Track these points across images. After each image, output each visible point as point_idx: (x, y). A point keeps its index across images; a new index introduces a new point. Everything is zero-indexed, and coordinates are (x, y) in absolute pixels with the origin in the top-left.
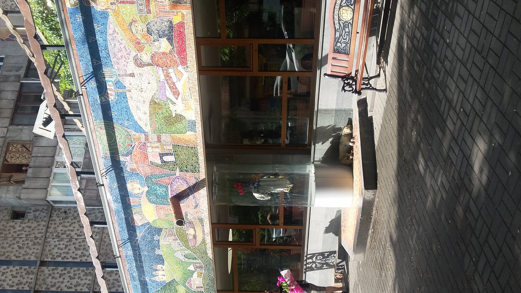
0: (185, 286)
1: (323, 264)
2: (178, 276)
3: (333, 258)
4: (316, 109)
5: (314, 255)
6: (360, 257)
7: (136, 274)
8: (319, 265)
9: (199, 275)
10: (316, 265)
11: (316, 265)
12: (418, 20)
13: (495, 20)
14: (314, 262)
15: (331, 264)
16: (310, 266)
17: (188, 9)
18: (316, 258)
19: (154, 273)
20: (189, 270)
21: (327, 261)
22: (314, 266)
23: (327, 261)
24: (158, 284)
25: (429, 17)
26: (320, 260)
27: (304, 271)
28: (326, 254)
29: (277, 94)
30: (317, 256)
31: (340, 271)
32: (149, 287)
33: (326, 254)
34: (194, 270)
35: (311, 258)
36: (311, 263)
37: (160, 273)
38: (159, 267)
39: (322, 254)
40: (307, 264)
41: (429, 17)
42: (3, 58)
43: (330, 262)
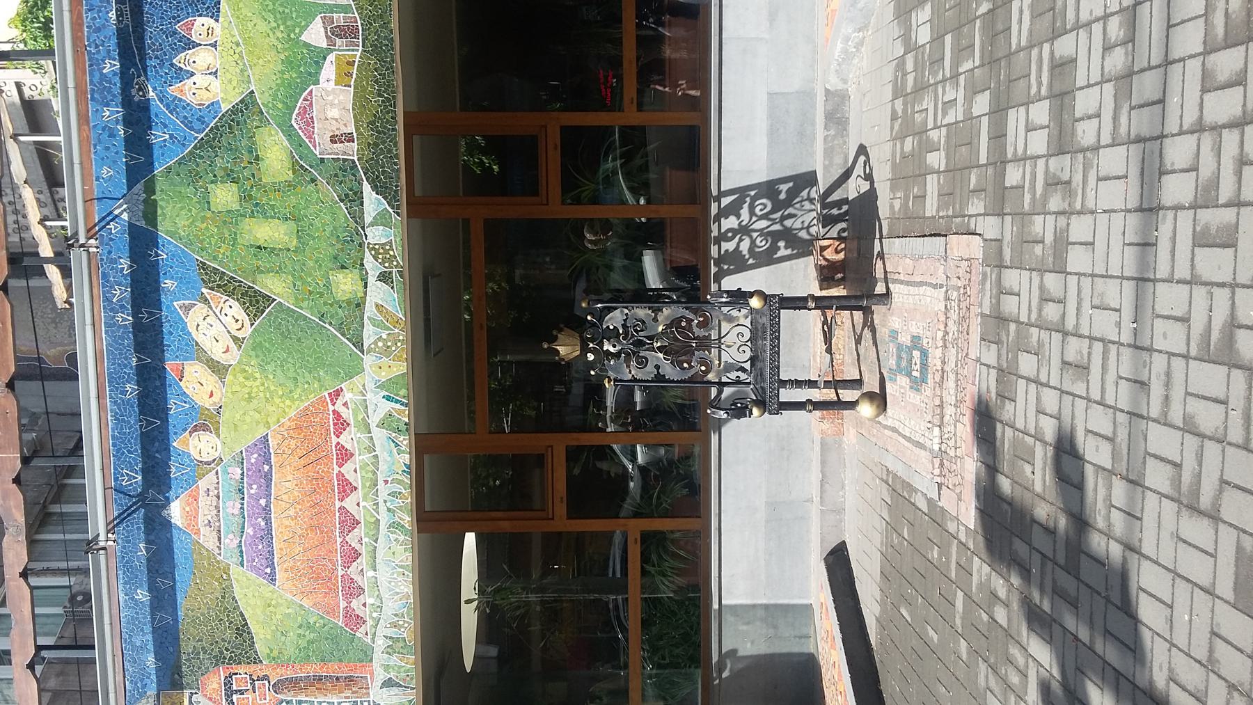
0: (289, 133)
1: (776, 236)
2: (264, 80)
3: (807, 205)
4: (716, 606)
5: (742, 191)
7: (111, 66)
8: (762, 245)
9: (343, 77)
10: (753, 242)
11: (753, 242)
14: (744, 230)
15: (803, 234)
16: (729, 246)
17: (398, 359)
18: (752, 213)
19: (179, 60)
20: (307, 45)
21: (788, 223)
22: (745, 246)
23: (788, 223)
24: (193, 117)
25: (953, 575)
26: (765, 217)
27: (713, 269)
29: (614, 572)
30: (754, 199)
32: (158, 136)
33: (784, 187)
34: (324, 45)
35: (734, 209)
37: (201, 58)
38: (202, 23)
39: (768, 189)
40: (722, 237)
41: (953, 575)
43: (798, 225)
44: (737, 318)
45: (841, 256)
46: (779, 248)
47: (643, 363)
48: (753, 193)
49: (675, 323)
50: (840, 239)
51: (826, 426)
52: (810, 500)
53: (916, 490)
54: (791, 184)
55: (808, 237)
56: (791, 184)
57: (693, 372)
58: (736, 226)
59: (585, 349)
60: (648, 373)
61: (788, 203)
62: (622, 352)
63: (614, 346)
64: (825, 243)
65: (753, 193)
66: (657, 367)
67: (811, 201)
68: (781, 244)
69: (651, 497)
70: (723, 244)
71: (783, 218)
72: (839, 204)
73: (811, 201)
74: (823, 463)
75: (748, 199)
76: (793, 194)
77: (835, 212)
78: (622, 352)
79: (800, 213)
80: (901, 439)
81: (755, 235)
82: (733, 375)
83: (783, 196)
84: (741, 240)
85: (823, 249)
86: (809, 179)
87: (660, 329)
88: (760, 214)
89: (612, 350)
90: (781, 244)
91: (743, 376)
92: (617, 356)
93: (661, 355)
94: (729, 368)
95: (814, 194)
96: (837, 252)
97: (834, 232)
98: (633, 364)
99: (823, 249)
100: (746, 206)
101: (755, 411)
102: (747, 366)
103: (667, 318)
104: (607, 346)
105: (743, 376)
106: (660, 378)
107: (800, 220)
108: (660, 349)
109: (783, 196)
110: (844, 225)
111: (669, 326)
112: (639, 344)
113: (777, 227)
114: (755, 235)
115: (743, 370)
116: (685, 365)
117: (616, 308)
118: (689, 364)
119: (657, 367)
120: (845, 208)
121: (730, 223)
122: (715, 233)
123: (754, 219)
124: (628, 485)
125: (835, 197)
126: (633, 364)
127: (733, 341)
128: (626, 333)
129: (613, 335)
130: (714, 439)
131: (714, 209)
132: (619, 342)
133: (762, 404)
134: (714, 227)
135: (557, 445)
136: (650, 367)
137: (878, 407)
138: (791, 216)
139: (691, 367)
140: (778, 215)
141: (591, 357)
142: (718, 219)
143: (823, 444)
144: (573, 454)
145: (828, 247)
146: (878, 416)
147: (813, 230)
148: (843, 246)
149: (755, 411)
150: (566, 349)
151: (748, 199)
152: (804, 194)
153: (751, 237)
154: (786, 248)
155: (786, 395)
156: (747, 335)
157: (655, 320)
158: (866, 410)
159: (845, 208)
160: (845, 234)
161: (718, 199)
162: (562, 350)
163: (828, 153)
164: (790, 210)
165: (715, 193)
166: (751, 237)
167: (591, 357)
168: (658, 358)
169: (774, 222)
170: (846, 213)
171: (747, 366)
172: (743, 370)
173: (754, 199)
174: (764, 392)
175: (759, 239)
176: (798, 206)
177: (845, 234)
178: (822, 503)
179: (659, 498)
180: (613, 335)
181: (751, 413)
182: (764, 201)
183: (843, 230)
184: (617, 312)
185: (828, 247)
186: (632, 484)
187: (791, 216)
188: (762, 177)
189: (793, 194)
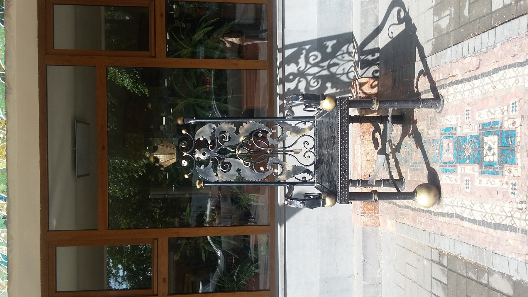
1: (324, 79)
5: (300, 46)
6: (405, 219)
10: (308, 83)
11: (308, 83)
12: (415, 81)
13: (434, 278)
14: (302, 74)
15: (344, 78)
18: (307, 62)
21: (333, 69)
22: (302, 87)
23: (333, 69)
26: (316, 65)
27: (279, 103)
28: (330, 44)
30: (308, 52)
31: (369, 72)
33: (330, 44)
35: (294, 59)
36: (295, 75)
39: (319, 44)
42: (211, 238)
43: (340, 71)
44: (303, 130)
45: (375, 90)
46: (326, 88)
47: (226, 167)
48: (307, 47)
49: (253, 134)
50: (374, 77)
51: (366, 219)
52: (352, 276)
53: (490, 272)
54: (335, 42)
55: (347, 80)
56: (335, 42)
57: (268, 174)
58: (295, 71)
59: (180, 157)
60: (232, 175)
61: (333, 55)
62: (210, 157)
63: (204, 154)
64: (363, 80)
65: (307, 47)
66: (239, 170)
67: (349, 54)
68: (329, 85)
69: (232, 276)
70: (286, 84)
71: (330, 66)
72: (372, 52)
73: (349, 54)
74: (365, 247)
75: (304, 52)
76: (336, 48)
77: (370, 57)
78: (210, 157)
79: (341, 63)
80: (466, 224)
81: (309, 78)
82: (300, 176)
83: (329, 50)
84: (299, 81)
85: (361, 85)
86: (348, 38)
87: (241, 139)
88: (312, 62)
89: (202, 157)
90: (329, 85)
91: (308, 177)
92: (205, 163)
93: (242, 161)
94: (296, 170)
95: (351, 49)
96: (372, 87)
97: (369, 73)
98: (219, 168)
99: (361, 85)
100: (303, 57)
101: (328, 201)
102: (312, 168)
103: (246, 131)
104: (199, 155)
105: (308, 177)
106: (241, 180)
107: (342, 68)
108: (241, 156)
109: (329, 50)
110: (376, 68)
111: (248, 137)
112: (224, 152)
113: (325, 72)
114: (309, 78)
115: (308, 172)
116: (262, 168)
117: (203, 124)
118: (265, 168)
119: (239, 170)
120: (377, 55)
121: (291, 69)
122: (280, 75)
123: (309, 66)
124: (218, 262)
125: (370, 46)
126: (219, 168)
127: (298, 150)
128: (213, 142)
129: (202, 145)
130: (280, 230)
131: (279, 58)
132: (208, 151)
133: (333, 194)
134: (279, 72)
135: (163, 236)
136: (233, 171)
137: (435, 196)
138: (335, 64)
139: (266, 170)
140: (325, 64)
141: (185, 163)
142: (282, 65)
143: (364, 233)
144: (173, 245)
145: (365, 83)
146: (433, 205)
147: (351, 75)
148: (376, 83)
149: (328, 201)
150: (165, 158)
151: (304, 52)
152: (345, 48)
153: (306, 79)
154: (332, 87)
155: (353, 189)
156: (312, 143)
157: (237, 132)
158: (423, 199)
159: (377, 55)
160: (377, 75)
161: (282, 50)
162: (162, 158)
163: (364, 14)
164: (335, 60)
165: (279, 44)
166: (306, 79)
167: (185, 163)
168: (239, 164)
169: (323, 68)
170: (378, 59)
171: (312, 168)
172: (308, 172)
173: (308, 52)
174: (332, 183)
175: (312, 81)
176: (340, 57)
177: (377, 75)
178: (364, 279)
179: (238, 276)
180: (202, 145)
181: (324, 203)
182: (316, 53)
183: (376, 71)
184: (206, 128)
185: (365, 83)
186: (219, 261)
187: (335, 64)
188: (314, 35)
189: (336, 48)
